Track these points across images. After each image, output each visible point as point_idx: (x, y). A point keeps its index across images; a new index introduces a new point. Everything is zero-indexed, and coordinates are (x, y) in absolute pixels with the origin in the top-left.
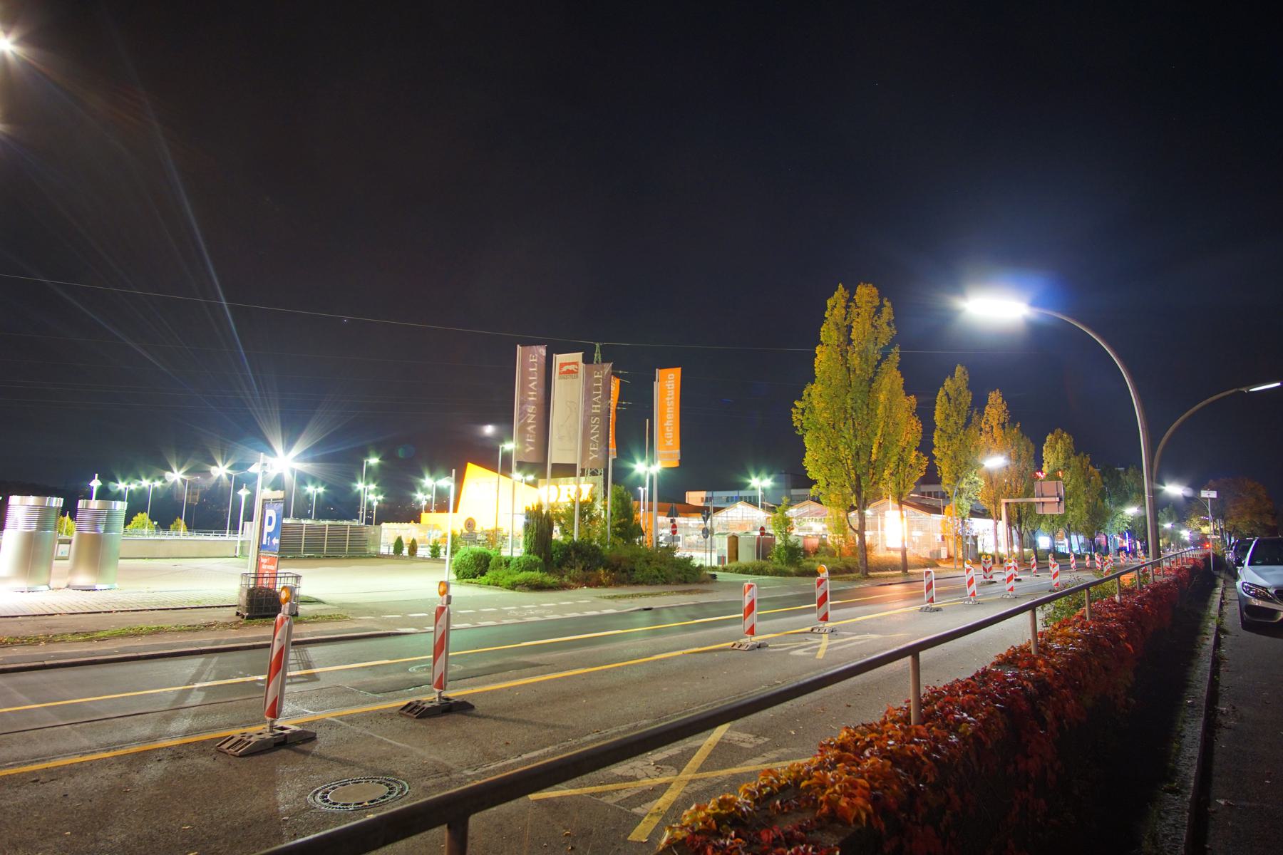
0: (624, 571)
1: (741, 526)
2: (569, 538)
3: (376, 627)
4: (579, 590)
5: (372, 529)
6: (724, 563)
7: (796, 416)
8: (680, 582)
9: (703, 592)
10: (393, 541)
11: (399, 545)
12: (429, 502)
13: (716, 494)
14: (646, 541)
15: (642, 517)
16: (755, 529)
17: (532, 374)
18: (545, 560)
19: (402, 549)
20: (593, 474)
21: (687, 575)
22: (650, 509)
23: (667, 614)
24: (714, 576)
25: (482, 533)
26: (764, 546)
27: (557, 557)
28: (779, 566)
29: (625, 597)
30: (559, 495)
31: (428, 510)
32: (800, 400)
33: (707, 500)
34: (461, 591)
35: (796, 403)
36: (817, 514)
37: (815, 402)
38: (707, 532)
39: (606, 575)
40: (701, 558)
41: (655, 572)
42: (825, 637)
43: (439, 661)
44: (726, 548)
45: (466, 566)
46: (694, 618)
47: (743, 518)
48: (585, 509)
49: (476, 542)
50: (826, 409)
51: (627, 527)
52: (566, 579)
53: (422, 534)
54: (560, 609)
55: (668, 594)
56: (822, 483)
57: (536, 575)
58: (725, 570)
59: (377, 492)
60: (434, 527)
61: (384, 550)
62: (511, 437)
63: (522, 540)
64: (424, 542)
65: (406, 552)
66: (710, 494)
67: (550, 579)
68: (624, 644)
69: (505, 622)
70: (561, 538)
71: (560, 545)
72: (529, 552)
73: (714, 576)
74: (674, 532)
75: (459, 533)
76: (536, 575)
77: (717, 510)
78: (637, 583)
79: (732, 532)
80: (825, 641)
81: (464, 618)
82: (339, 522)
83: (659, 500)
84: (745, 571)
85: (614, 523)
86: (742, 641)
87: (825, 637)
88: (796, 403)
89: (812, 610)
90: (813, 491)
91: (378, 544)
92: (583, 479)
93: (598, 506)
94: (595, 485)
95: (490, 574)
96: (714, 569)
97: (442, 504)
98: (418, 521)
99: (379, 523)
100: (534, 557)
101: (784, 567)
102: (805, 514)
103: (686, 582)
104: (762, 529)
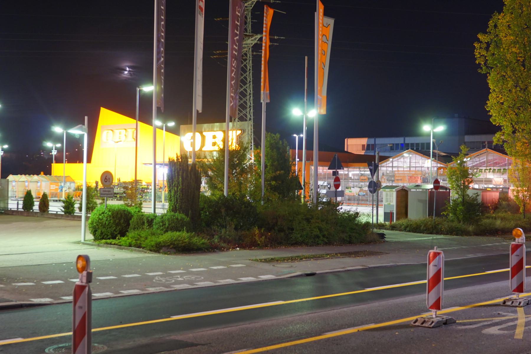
0: (281, 230)
1: (411, 178)
2: (218, 193)
3: (6, 296)
4: (231, 252)
6: (391, 220)
7: (479, 52)
8: (344, 242)
10: (21, 194)
11: (28, 199)
12: (60, 151)
13: (380, 141)
14: (305, 196)
15: (299, 167)
16: (425, 181)
17: (162, 20)
18: (192, 218)
21: (353, 235)
22: (309, 158)
23: (333, 281)
24: (382, 236)
25: (120, 185)
26: (437, 200)
27: (202, 213)
28: (455, 224)
29: (284, 260)
30: (210, 141)
31: (59, 160)
32: (485, 32)
33: (369, 147)
34: (102, 254)
35: (480, 36)
36: (495, 164)
37: (502, 35)
38: (374, 187)
39: (261, 235)
40: (366, 213)
41: (316, 232)
42: (520, 311)
43: (79, 349)
44: (394, 203)
45: (104, 226)
46: (364, 286)
47: (411, 168)
48: (234, 159)
49: (114, 196)
50: (515, 43)
51: (283, 181)
52: (216, 240)
53: (53, 187)
56: (507, 129)
57: (183, 235)
58: (393, 228)
60: (67, 179)
61: (12, 205)
62: (150, 80)
63: (164, 193)
65: (36, 207)
66: (372, 141)
67: (198, 240)
68: (288, 318)
69: (152, 290)
70: (208, 194)
71: (207, 200)
72: (174, 209)
75: (93, 185)
76: (183, 235)
77: (383, 159)
78: (296, 244)
79: (401, 184)
80: (521, 317)
81: (105, 286)
83: (320, 149)
84: (416, 229)
85: (269, 176)
86: (425, 315)
87: (520, 311)
88: (480, 36)
89: (503, 277)
90: (496, 138)
92: (231, 124)
93: (251, 158)
94: (243, 131)
95: (131, 234)
97: (74, 153)
98: (48, 172)
100: (179, 216)
101: (461, 225)
102: (482, 164)
103: (350, 243)
104: (436, 182)
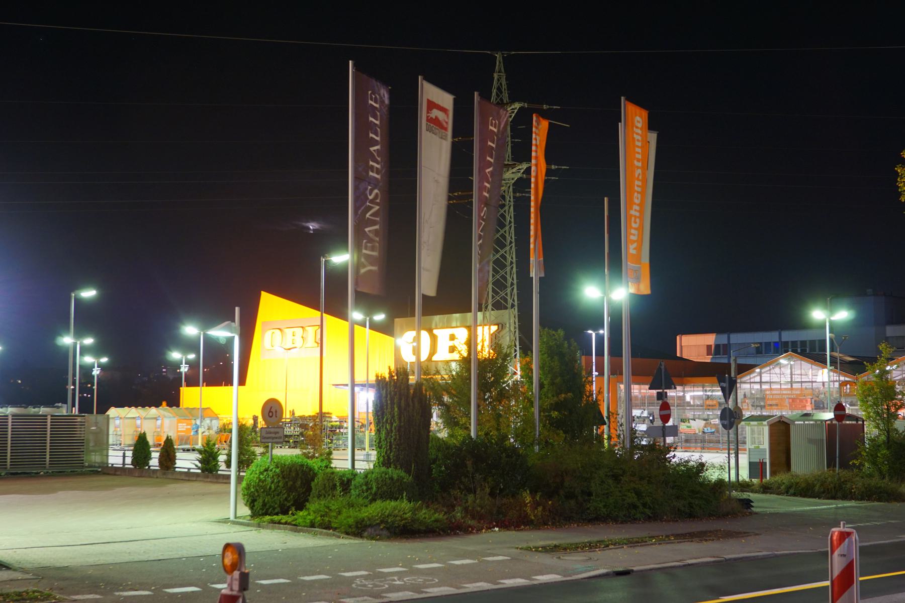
0: (570, 496)
1: (795, 401)
2: (460, 433)
4: (485, 535)
5: (92, 418)
6: (762, 475)
9: (729, 535)
10: (129, 440)
11: (141, 447)
12: (193, 365)
13: (737, 338)
15: (599, 385)
16: (820, 406)
19: (148, 457)
20: (498, 306)
21: (695, 502)
22: (616, 370)
28: (876, 481)
29: (618, 544)
30: (445, 344)
31: (192, 382)
33: (718, 349)
34: (264, 540)
39: (536, 505)
40: (717, 464)
41: (632, 498)
44: (766, 445)
45: (268, 492)
48: (486, 373)
49: (284, 440)
51: (571, 409)
53: (183, 427)
54: (450, 575)
55: (665, 539)
57: (403, 507)
58: (766, 489)
59: (96, 351)
61: (115, 458)
63: (369, 435)
64: (185, 440)
66: (723, 339)
67: (427, 515)
70: (443, 434)
71: (443, 446)
72: (385, 462)
73: (747, 503)
74: (665, 418)
78: (597, 519)
82: (32, 410)
83: (634, 354)
84: (805, 490)
85: (547, 403)
91: (103, 445)
92: (480, 315)
93: (515, 372)
94: (501, 326)
95: (314, 505)
96: (743, 486)
97: (218, 370)
98: (174, 402)
99: (103, 410)
100: (395, 473)
104: (839, 408)
